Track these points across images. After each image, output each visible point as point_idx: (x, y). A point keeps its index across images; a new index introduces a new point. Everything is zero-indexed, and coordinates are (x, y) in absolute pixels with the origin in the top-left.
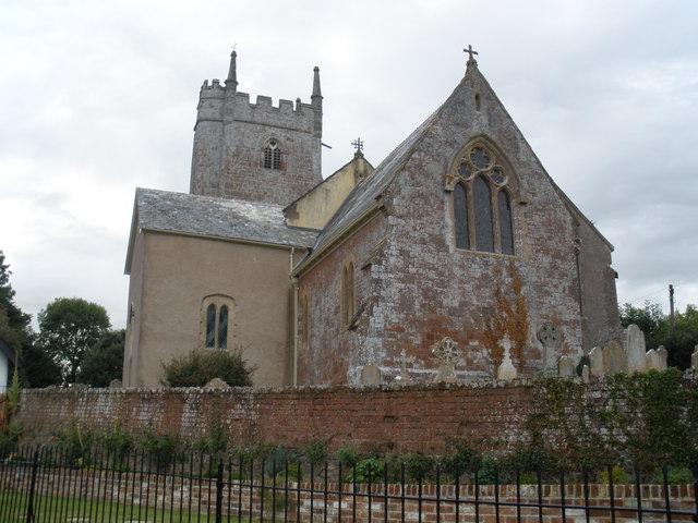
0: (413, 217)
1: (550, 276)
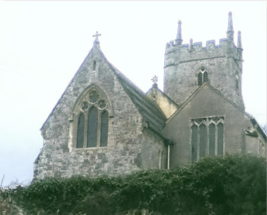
0: (54, 137)
1: (123, 155)
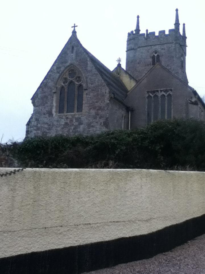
1: (94, 119)
